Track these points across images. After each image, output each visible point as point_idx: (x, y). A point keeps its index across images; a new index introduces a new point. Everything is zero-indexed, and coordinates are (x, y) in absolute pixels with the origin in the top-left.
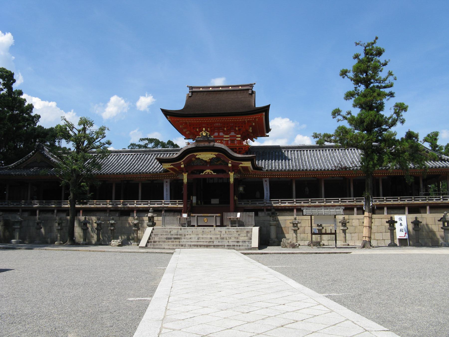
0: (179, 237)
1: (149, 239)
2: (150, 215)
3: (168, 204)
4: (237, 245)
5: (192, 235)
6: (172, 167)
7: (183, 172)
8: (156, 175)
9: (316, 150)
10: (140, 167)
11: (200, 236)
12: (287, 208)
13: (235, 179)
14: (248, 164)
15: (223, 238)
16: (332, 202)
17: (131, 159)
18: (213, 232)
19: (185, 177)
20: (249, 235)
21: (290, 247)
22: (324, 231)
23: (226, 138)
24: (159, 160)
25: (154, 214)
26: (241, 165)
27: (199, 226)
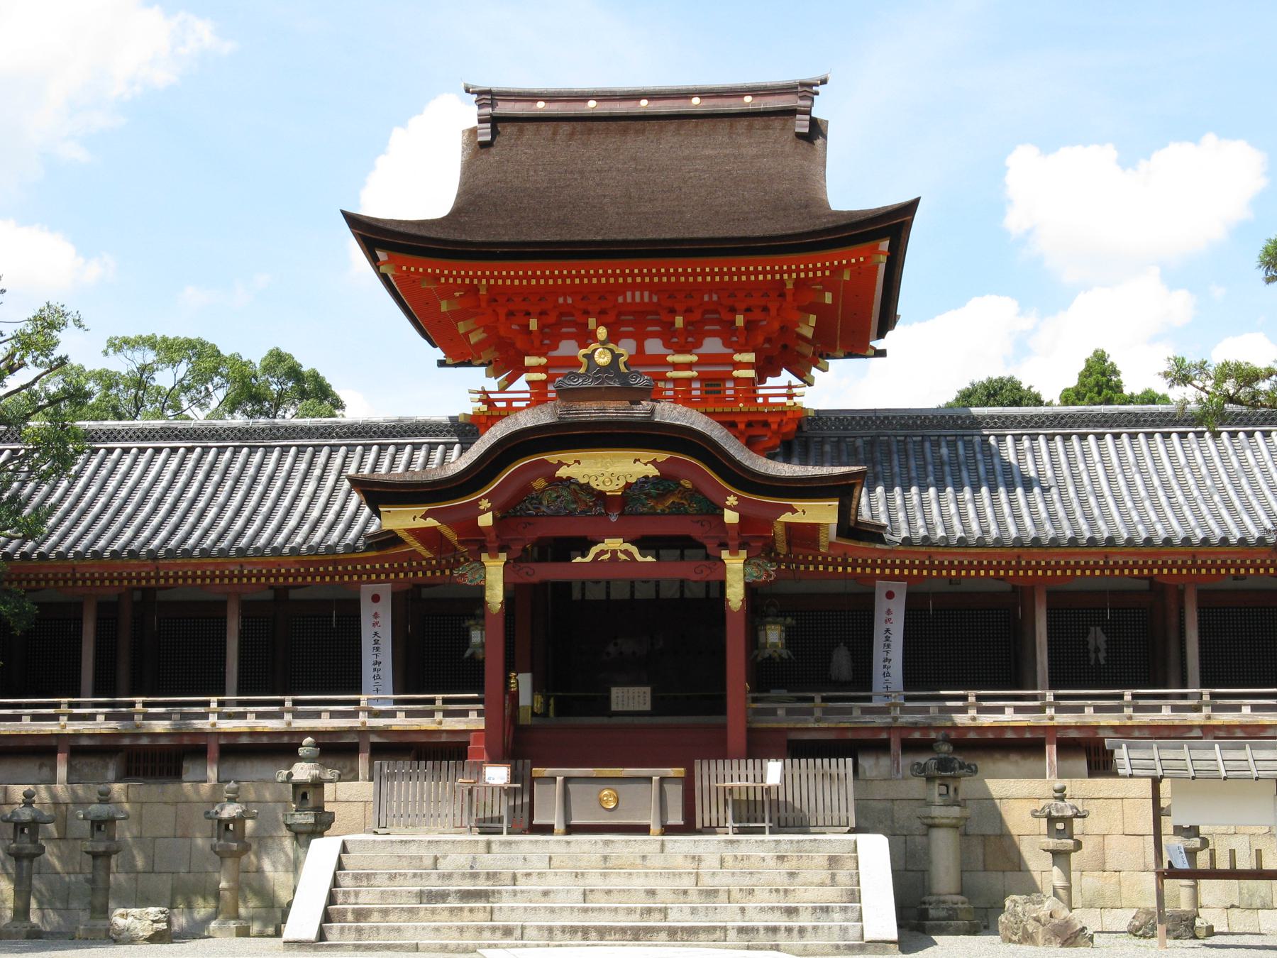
0: (482, 885)
1: (332, 899)
2: (303, 771)
3: (392, 714)
4: (789, 930)
5: (550, 879)
6: (431, 522)
7: (483, 548)
8: (326, 563)
9: (1149, 436)
10: (232, 521)
11: (594, 881)
12: (1010, 735)
13: (750, 588)
14: (822, 513)
15: (711, 893)
16: (1246, 710)
17: (176, 474)
18: (656, 861)
19: (494, 579)
20: (843, 875)
21: (1048, 942)
22: (1203, 861)
23: (676, 366)
24: (358, 484)
25: (324, 766)
26: (787, 517)
27: (571, 829)
